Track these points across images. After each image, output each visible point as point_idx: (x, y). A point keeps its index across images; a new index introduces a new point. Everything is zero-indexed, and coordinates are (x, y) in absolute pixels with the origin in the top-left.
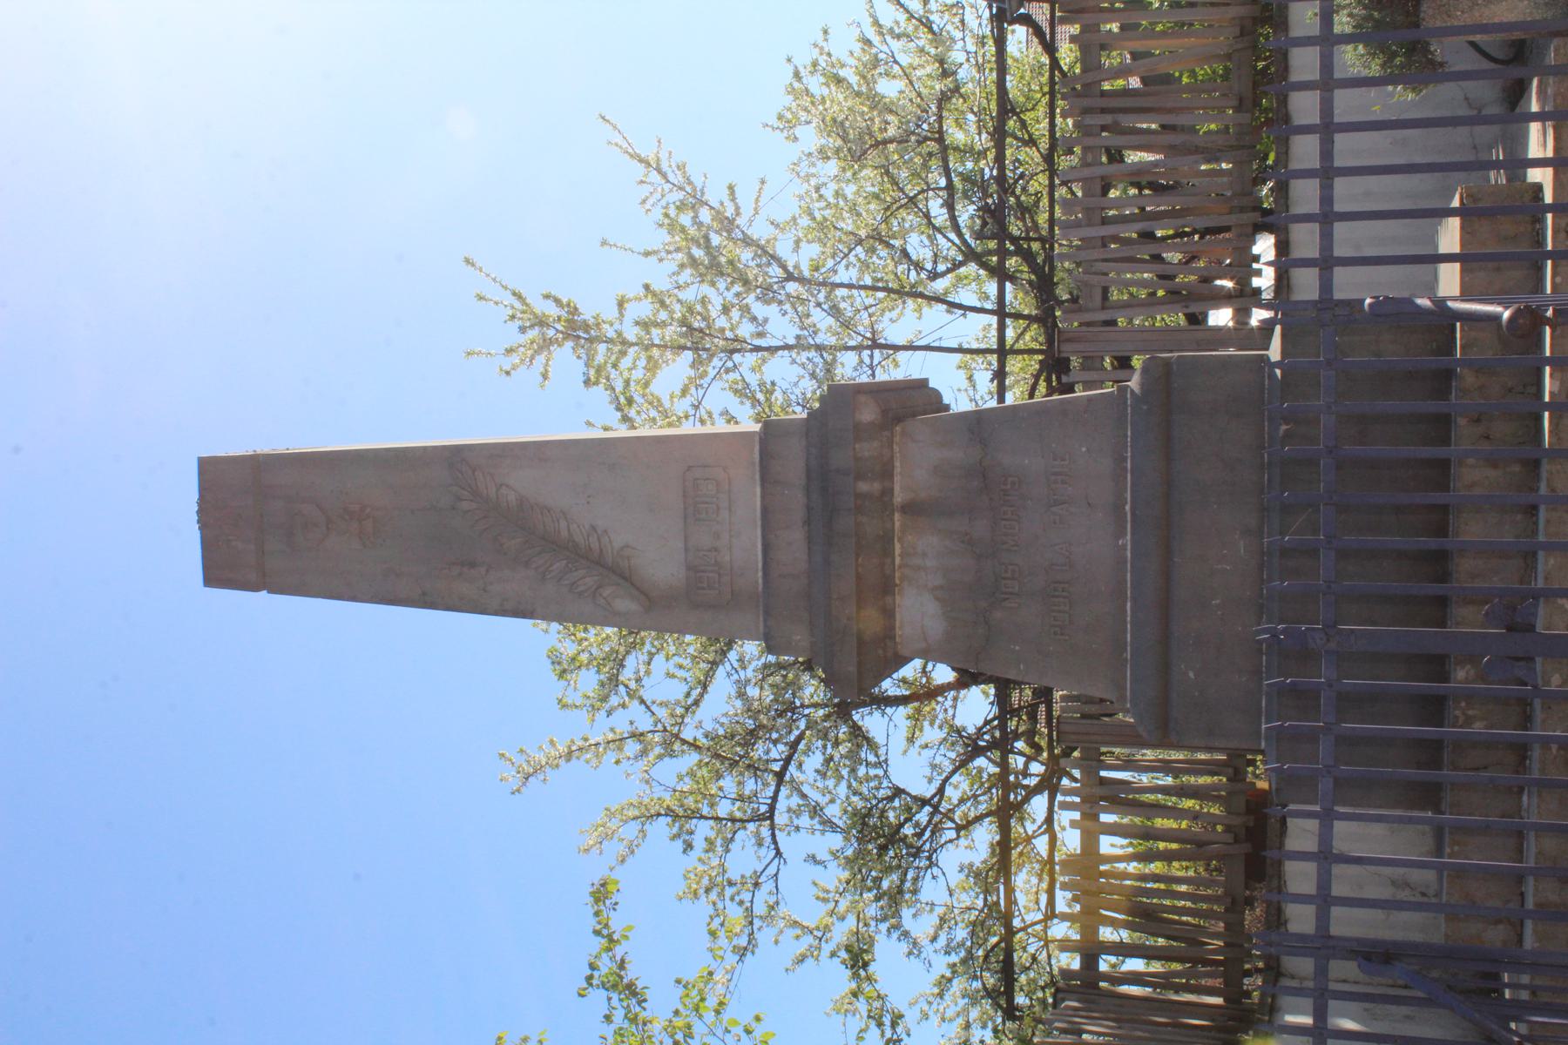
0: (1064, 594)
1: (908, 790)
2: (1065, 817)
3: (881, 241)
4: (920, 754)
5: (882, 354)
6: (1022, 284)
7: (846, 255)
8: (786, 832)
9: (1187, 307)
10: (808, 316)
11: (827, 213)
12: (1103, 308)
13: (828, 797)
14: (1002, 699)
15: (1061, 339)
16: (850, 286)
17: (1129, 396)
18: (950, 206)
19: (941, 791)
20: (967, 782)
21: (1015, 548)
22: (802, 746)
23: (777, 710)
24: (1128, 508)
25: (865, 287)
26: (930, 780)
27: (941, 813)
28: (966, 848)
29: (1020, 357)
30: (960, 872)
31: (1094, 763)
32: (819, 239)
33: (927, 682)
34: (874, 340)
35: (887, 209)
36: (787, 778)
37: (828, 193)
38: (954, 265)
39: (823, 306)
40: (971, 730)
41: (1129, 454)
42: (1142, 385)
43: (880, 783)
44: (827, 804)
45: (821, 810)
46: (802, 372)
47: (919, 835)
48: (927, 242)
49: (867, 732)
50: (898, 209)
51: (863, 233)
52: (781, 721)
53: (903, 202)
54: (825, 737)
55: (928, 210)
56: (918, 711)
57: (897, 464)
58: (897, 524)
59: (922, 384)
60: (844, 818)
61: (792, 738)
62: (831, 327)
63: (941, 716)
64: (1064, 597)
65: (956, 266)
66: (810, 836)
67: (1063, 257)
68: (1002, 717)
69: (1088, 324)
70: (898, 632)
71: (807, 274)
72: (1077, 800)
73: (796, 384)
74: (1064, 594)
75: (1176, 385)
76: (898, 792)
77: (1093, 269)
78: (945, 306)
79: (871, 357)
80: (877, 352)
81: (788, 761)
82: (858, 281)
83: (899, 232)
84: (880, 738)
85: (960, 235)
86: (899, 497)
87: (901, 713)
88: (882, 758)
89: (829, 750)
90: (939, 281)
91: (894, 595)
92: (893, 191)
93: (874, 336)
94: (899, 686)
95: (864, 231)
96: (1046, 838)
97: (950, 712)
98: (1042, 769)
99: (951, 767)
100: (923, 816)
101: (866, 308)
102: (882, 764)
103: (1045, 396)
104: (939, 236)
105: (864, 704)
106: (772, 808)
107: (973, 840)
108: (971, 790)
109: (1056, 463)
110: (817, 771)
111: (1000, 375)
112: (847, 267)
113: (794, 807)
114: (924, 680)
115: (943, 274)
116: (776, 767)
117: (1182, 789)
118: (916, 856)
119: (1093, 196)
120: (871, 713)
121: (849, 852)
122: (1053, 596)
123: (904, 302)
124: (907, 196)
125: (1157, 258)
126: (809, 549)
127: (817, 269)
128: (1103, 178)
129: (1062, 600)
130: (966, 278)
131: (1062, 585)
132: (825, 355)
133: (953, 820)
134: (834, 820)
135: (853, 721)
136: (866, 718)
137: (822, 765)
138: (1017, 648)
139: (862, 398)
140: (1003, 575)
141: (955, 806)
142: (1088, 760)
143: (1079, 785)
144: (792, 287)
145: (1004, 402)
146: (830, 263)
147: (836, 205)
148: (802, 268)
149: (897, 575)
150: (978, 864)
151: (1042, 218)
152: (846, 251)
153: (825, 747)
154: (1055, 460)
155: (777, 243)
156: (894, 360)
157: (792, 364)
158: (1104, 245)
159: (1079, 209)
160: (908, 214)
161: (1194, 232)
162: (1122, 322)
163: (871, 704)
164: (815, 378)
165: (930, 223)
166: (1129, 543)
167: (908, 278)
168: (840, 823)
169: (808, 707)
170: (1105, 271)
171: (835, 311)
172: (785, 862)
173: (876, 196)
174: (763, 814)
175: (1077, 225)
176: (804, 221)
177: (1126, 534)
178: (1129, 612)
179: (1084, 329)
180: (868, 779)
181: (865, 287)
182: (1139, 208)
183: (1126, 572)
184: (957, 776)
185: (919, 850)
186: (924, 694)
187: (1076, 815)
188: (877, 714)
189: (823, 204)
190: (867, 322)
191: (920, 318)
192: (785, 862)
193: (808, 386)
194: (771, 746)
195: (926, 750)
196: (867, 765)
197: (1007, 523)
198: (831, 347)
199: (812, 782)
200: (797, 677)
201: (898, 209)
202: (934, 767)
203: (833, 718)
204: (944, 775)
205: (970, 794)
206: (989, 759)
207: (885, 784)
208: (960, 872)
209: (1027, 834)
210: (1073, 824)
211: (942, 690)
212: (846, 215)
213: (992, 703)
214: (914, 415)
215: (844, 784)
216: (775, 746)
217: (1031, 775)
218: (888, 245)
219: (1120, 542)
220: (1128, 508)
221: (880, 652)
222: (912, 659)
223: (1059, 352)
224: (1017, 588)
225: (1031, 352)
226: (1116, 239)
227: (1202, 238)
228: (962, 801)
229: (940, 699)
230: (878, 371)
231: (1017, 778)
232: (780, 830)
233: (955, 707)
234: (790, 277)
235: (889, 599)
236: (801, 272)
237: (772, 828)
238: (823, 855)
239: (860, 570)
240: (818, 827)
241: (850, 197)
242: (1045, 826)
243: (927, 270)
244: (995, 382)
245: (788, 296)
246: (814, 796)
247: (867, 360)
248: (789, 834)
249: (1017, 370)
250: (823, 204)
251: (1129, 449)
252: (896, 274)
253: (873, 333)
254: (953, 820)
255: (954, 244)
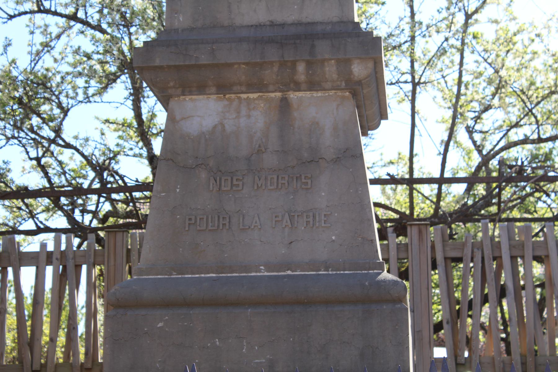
0: (221, 226)
1: (67, 118)
2: (49, 238)
3: (497, 89)
4: (97, 129)
5: (408, 92)
6: (464, 198)
7: (486, 60)
8: (29, 24)
9: (448, 323)
10: (438, 32)
11: (519, 46)
12: (446, 259)
13: (59, 57)
14: (142, 186)
15: (422, 227)
16: (461, 64)
17: (376, 271)
18: (525, 141)
19: (68, 146)
20: (75, 167)
21: (256, 188)
22: (98, 35)
23: (126, 13)
24: (289, 272)
25: (460, 76)
26: (76, 138)
27: (50, 146)
28: (23, 167)
29: (408, 200)
30: (4, 161)
31: (92, 260)
32: (498, 39)
33: (153, 134)
34: (419, 83)
35: (522, 91)
36: (72, 23)
37: (537, 46)
38: (479, 146)
39: (446, 43)
40: (116, 167)
41: (330, 273)
42: (384, 281)
43: (72, 98)
44: (53, 56)
45: (48, 51)
46: (393, 26)
47: (32, 130)
48: (497, 125)
49: (112, 87)
50: (523, 101)
51: (503, 73)
52: (118, 17)
53: (528, 104)
54: (106, 52)
55: (521, 126)
56: (130, 126)
57: (320, 94)
58: (273, 95)
59: (383, 115)
60: (42, 70)
61: (104, 26)
62: (429, 52)
63: (126, 144)
64: (218, 226)
65: (479, 149)
66: (27, 43)
67: (485, 230)
68: (125, 189)
69: (433, 247)
70: (188, 98)
71: (471, 30)
72: (63, 247)
73: (383, 22)
74: (221, 226)
75: (385, 307)
76: (65, 112)
77: (475, 250)
78: (446, 138)
79: (406, 82)
80: (409, 87)
81: (85, 23)
82: (465, 69)
83: (505, 103)
84: (106, 97)
85: (502, 149)
86: (293, 96)
87: (129, 115)
88: (91, 99)
89: (96, 57)
90: (466, 135)
91: (217, 94)
92: (537, 97)
93: (422, 83)
94: (149, 112)
95: (505, 74)
96: (34, 227)
97: (131, 153)
98: (87, 222)
99: (86, 154)
100: (47, 132)
101: (443, 77)
102: (88, 99)
103: (377, 216)
104: (501, 134)
105: (133, 82)
106: (47, 12)
107: (29, 172)
108: (69, 170)
109: (323, 217)
110: (79, 48)
111: (393, 180)
112: (477, 62)
113: (49, 30)
114: (155, 131)
115: (471, 138)
116: (81, 14)
117: (74, 328)
118: (15, 126)
119: (533, 250)
120: (126, 88)
121: (15, 73)
122: (219, 217)
123: (449, 108)
124: (532, 108)
125: (485, 299)
126: (252, 26)
127: (475, 37)
128: (547, 256)
129: (216, 225)
130: (469, 158)
131: (227, 224)
132: (407, 45)
133: (43, 156)
134: (40, 62)
135: (121, 75)
136: (123, 84)
137: (84, 52)
138: (178, 190)
139: (371, 65)
140: (235, 178)
141: (56, 158)
142: (95, 255)
143: (75, 249)
144: (460, 18)
145: (371, 184)
146: (479, 48)
147: (525, 53)
148: (476, 26)
149: (233, 96)
150: (10, 176)
151: (516, 214)
152: (489, 61)
153: (98, 53)
154: (325, 215)
155: (495, 5)
156: (404, 100)
157: (399, 18)
158: (494, 259)
159: (523, 238)
160: (519, 110)
161: (508, 334)
162: (435, 277)
163: (134, 88)
164: (388, 36)
165: (512, 127)
166: (261, 274)
167: (468, 111)
168: (38, 67)
169: (130, 38)
170: (475, 260)
171: (442, 52)
172: (4, 23)
173: (532, 84)
174: (42, 5)
175: (510, 238)
176: (513, 27)
177: (267, 272)
178: (208, 275)
179: (429, 245)
180: (74, 88)
181: (460, 76)
182: (524, 285)
183: (246, 273)
184: (81, 158)
185: (20, 129)
186: (144, 130)
187: (51, 247)
188: (126, 93)
189: (527, 43)
190: (433, 78)
191: (437, 122)
192: (4, 23)
193: (381, 32)
194: (97, 9)
195: (99, 134)
196: (86, 88)
197: (275, 180)
198: (413, 50)
199: (70, 44)
200: (153, 28)
201: (523, 101)
202: (87, 140)
203: (122, 57)
204: (81, 149)
205: (66, 169)
206: (93, 181)
207: (71, 101)
208: (4, 161)
209: (36, 214)
210: (43, 246)
211: (148, 145)
212: (518, 60)
213: (137, 181)
214: (358, 107)
215: (70, 69)
216: (97, 12)
217: (83, 216)
218: (494, 95)
219: (262, 267)
220: (289, 272)
221: (172, 84)
222: (167, 110)
223: (411, 225)
224: (225, 189)
225: (412, 208)
226: (500, 267)
227: (502, 339)
228: (60, 163)
229: (141, 144)
230: (395, 88)
231: (81, 205)
232: (31, 19)
233: (135, 156)
234: (468, 16)
235: (213, 90)
236: (472, 25)
237: (32, 12)
238: (12, 53)
239: (236, 66)
240: (34, 50)
241: (532, 64)
242: (42, 226)
243: (474, 126)
244: (388, 177)
245: (453, 14)
246: (59, 46)
247: (403, 79)
248: (28, 26)
249: (398, 197)
250: (527, 43)
251: (335, 272)
252: (471, 101)
253: (425, 83)
254: (43, 156)
255: (495, 146)
